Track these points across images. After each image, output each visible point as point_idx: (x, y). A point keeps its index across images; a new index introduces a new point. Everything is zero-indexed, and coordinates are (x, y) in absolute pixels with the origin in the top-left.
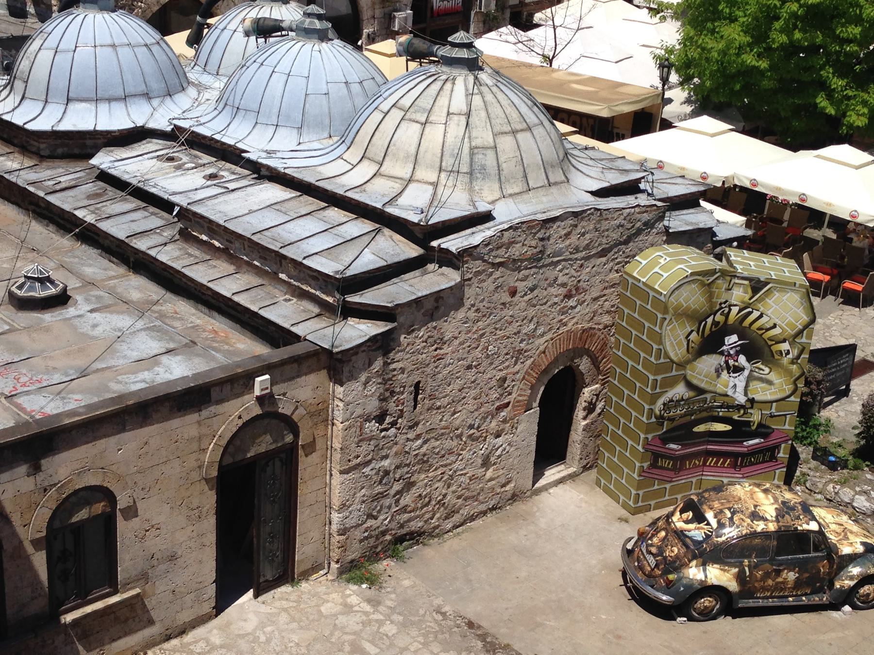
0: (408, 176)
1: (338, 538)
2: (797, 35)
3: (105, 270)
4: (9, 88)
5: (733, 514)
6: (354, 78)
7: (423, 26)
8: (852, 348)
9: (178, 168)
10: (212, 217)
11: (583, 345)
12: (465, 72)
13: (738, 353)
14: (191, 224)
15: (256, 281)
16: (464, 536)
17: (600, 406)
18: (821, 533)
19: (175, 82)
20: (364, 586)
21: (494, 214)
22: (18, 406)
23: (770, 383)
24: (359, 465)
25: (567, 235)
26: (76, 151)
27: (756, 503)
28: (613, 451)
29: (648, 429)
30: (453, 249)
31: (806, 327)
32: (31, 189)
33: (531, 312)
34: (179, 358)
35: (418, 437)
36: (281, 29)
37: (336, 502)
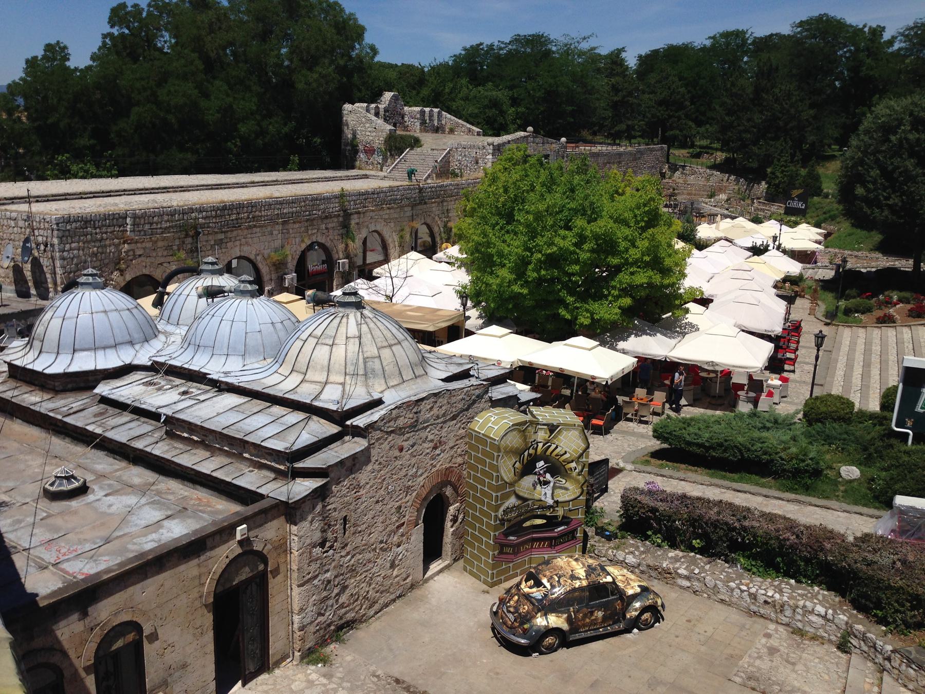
0: (325, 380)
1: (299, 633)
2: (543, 272)
3: (111, 465)
4: (29, 346)
5: (559, 578)
6: (277, 319)
7: (303, 282)
8: (606, 461)
9: (159, 389)
10: (191, 421)
11: (447, 479)
12: (354, 310)
13: (545, 473)
14: (174, 427)
15: (228, 460)
16: (383, 618)
17: (461, 517)
18: (614, 582)
19: (149, 333)
20: (320, 665)
21: (384, 399)
22: (62, 570)
23: (566, 489)
24: (310, 579)
25: (431, 408)
26: (82, 385)
27: (571, 569)
28: (473, 547)
29: (496, 528)
30: (361, 425)
31: (584, 451)
32: (51, 414)
33: (413, 460)
34: (176, 521)
35: (348, 554)
36: (224, 292)
37: (296, 608)
